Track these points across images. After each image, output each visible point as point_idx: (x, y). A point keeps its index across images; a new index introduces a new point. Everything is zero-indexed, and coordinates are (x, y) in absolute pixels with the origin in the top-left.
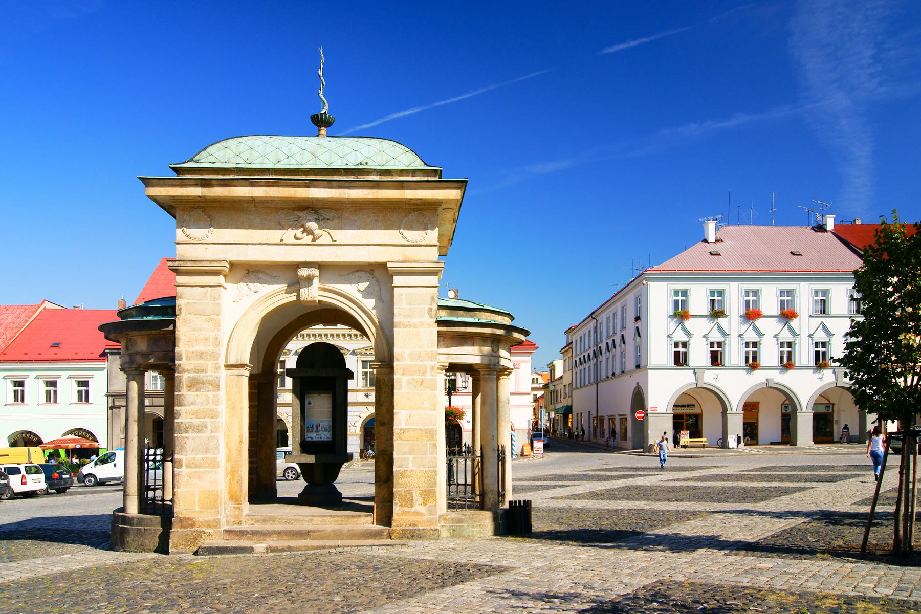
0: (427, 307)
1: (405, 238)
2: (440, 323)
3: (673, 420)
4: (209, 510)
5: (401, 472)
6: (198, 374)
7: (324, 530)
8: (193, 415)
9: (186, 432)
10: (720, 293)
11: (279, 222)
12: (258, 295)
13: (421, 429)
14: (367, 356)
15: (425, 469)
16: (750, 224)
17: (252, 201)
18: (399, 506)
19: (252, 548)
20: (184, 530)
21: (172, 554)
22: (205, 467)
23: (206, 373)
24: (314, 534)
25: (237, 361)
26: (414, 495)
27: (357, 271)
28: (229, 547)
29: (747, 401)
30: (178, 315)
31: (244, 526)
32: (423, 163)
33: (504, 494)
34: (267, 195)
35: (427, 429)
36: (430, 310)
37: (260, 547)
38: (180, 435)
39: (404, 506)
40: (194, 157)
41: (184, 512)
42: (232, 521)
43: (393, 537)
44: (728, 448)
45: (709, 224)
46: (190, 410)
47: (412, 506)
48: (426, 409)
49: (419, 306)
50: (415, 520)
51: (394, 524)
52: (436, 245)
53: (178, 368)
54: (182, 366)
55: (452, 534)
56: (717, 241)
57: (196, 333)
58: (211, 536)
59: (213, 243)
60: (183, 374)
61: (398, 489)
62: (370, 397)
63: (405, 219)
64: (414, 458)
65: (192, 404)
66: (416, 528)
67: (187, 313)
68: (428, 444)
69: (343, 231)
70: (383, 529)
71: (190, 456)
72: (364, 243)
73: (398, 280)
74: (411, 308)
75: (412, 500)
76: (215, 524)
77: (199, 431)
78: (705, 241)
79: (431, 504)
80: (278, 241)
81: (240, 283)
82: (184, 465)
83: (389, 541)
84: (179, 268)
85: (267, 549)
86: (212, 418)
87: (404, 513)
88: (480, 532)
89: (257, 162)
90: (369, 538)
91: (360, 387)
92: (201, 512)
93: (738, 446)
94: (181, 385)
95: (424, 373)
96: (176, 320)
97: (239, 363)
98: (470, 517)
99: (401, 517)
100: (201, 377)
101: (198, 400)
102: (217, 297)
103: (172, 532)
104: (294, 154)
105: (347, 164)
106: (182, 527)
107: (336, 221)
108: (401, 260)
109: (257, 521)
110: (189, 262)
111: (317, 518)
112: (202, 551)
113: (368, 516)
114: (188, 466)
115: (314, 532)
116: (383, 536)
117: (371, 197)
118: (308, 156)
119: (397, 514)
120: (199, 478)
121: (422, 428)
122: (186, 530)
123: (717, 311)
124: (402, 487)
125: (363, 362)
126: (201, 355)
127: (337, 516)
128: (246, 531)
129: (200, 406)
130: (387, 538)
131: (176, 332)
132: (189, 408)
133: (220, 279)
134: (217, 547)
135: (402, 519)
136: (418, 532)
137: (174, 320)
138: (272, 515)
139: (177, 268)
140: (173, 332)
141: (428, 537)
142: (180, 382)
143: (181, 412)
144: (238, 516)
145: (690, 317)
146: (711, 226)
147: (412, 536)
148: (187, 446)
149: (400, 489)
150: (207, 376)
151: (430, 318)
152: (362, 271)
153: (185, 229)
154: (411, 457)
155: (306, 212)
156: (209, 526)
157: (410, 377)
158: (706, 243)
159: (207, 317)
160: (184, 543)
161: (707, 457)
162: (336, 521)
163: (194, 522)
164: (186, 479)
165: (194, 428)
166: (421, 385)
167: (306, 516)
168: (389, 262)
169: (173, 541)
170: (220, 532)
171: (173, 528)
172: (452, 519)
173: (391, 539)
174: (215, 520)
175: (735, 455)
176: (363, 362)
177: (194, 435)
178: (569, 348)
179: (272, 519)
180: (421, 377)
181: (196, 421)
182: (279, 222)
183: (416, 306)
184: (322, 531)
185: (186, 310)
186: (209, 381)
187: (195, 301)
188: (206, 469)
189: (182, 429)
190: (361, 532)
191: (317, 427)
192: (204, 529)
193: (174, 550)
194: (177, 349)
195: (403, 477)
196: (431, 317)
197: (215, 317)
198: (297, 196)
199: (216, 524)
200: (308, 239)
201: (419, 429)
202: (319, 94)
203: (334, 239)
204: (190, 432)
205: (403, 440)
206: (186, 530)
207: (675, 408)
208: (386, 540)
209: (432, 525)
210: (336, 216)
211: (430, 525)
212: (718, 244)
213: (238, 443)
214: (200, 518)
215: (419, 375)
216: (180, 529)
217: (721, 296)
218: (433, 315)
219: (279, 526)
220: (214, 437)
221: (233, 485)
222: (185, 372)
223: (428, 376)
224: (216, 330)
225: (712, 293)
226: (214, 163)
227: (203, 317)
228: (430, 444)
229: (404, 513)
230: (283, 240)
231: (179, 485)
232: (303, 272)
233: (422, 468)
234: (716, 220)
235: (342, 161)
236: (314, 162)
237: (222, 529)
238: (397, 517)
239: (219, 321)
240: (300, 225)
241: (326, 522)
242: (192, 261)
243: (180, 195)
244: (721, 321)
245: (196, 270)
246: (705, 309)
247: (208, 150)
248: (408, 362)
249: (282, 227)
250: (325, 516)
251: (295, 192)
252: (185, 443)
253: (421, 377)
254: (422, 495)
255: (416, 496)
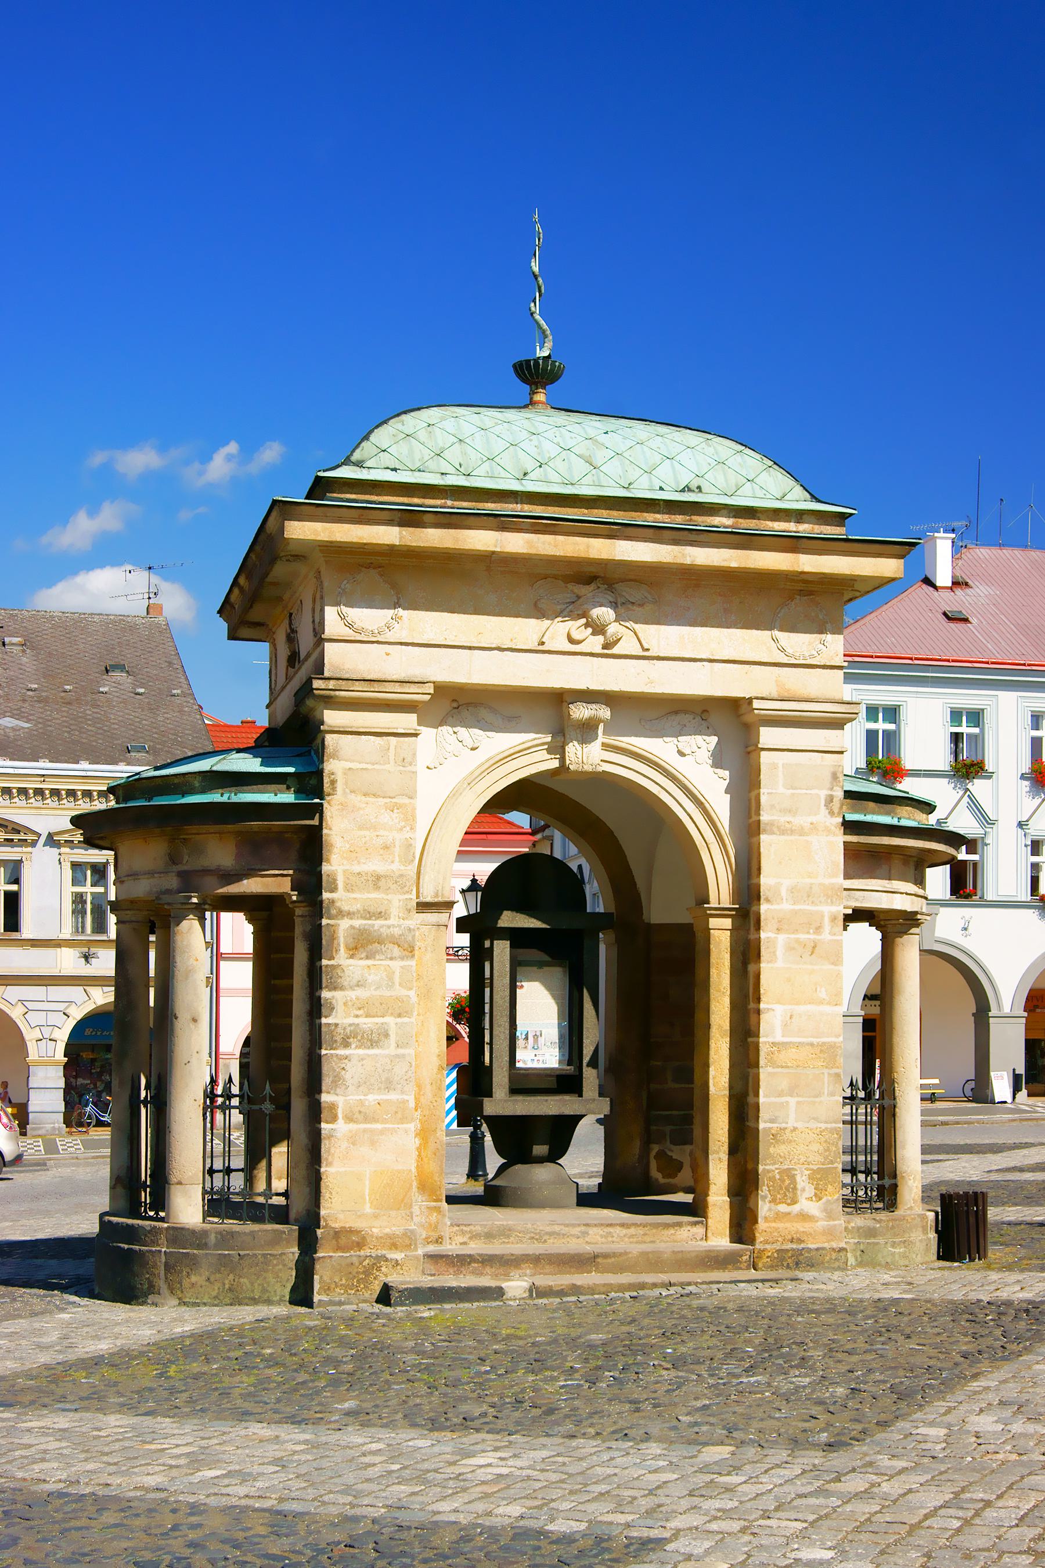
0: (823, 793)
1: (783, 650)
2: (849, 827)
3: (864, 1031)
4: (393, 1213)
5: (773, 1132)
6: (370, 922)
7: (626, 1253)
8: (360, 1009)
9: (346, 1045)
10: (976, 717)
11: (535, 605)
12: (480, 757)
13: (812, 1045)
14: (76, 851)
15: (820, 1125)
16: (1026, 547)
17: (489, 560)
18: (770, 1202)
19: (501, 1288)
20: (345, 1255)
21: (319, 1306)
22: (385, 1121)
23: (386, 919)
24: (605, 1261)
25: (437, 895)
26: (798, 1178)
27: (676, 712)
28: (453, 1288)
29: (1034, 988)
30: (329, 795)
31: (449, 1247)
32: (808, 494)
33: (896, 1186)
34: (533, 551)
35: (824, 1043)
36: (830, 799)
37: (516, 1286)
38: (332, 1052)
39: (778, 1201)
40: (351, 454)
41: (341, 1216)
42: (424, 1236)
43: (760, 1265)
44: (993, 1102)
45: (938, 541)
46: (354, 997)
47: (794, 1202)
48: (821, 1002)
49: (808, 792)
50: (802, 1229)
51: (760, 1238)
52: (841, 668)
53: (328, 909)
54: (338, 904)
55: (859, 1259)
56: (956, 583)
57: (367, 833)
58: (399, 1267)
59: (401, 644)
60: (339, 922)
61: (767, 1167)
62: (93, 961)
63: (783, 611)
64: (798, 1103)
65: (358, 986)
66: (802, 1246)
67: (348, 791)
68: (826, 1075)
69: (663, 628)
70: (742, 1250)
71: (354, 1097)
72: (704, 657)
73: (768, 736)
74: (793, 794)
75: (795, 1188)
76: (407, 1242)
77: (373, 1043)
78: (928, 582)
79: (830, 1198)
80: (533, 645)
81: (441, 725)
82: (340, 1115)
83: (752, 1274)
84: (337, 693)
85: (530, 1291)
86: (399, 1016)
87: (779, 1217)
88: (904, 1256)
89: (481, 471)
90: (713, 1269)
91: (67, 933)
92: (376, 1216)
93: (1014, 1098)
94: (335, 946)
95: (818, 929)
96: (326, 805)
97: (440, 899)
98: (888, 1227)
99: (774, 1225)
100: (376, 928)
101: (371, 978)
102: (408, 759)
103: (319, 1258)
104: (550, 459)
105: (661, 489)
106: (339, 1248)
107: (648, 607)
108: (775, 695)
109: (474, 1236)
110: (357, 683)
111: (595, 1229)
112: (400, 1297)
113: (695, 1224)
114: (349, 1119)
115: (606, 1256)
116: (741, 1262)
117: (734, 564)
118: (580, 467)
119: (766, 1218)
120: (373, 1143)
121: (815, 1041)
122: (348, 1255)
123: (968, 762)
124: (774, 1164)
125: (75, 866)
126: (377, 881)
127: (635, 1225)
128: (470, 1256)
129: (375, 989)
130: (748, 1268)
131: (325, 831)
132: (352, 994)
133: (407, 721)
134: (430, 1288)
135: (777, 1229)
136: (807, 1255)
137: (321, 805)
138: (505, 1223)
139: (332, 693)
140: (320, 828)
141: (826, 1265)
142: (333, 938)
143: (334, 1001)
144: (436, 1227)
145: (907, 775)
146: (943, 546)
147: (797, 1264)
148: (347, 1076)
149: (772, 1167)
150: (389, 927)
151: (829, 816)
152: (686, 712)
153: (344, 609)
154: (792, 1101)
155: (593, 586)
156: (394, 1246)
157: (793, 936)
158: (930, 588)
159: (388, 800)
160: (344, 1282)
161: (957, 1123)
162: (632, 1236)
163: (364, 1238)
164: (344, 1145)
165: (363, 1037)
166: (812, 953)
167: (574, 1225)
168: (757, 698)
169: (321, 1277)
170: (417, 1258)
171: (320, 1250)
172: (859, 1228)
173: (755, 1269)
174: (405, 1234)
175: (1021, 1120)
176: (75, 866)
177: (361, 1052)
178: (544, 838)
179: (505, 1232)
180: (812, 937)
181: (366, 1023)
182: (535, 605)
183: (804, 791)
184: (621, 1254)
185: (346, 783)
186: (393, 936)
187: (364, 766)
188: (387, 1126)
189: (338, 1038)
190: (697, 1256)
191: (536, 1037)
192: (384, 1252)
193: (325, 1298)
194: (326, 868)
195: (778, 1141)
196: (832, 813)
197: (406, 801)
198: (592, 557)
199: (405, 1241)
200: (595, 643)
201: (808, 1044)
202: (532, 314)
203: (646, 646)
204: (353, 1046)
205: (778, 1067)
206: (348, 1255)
207: (867, 1001)
208: (746, 1272)
209: (832, 1240)
210: (649, 596)
211: (828, 1241)
212: (959, 592)
213: (435, 1070)
214: (374, 1230)
215: (808, 933)
216: (334, 1252)
217: (977, 725)
218: (836, 810)
219: (519, 1245)
220: (404, 1056)
221: (426, 1160)
222: (343, 916)
223: (826, 936)
224: (408, 828)
225: (956, 715)
226: (395, 470)
227: (381, 799)
228: (829, 1074)
229: (779, 1217)
230: (543, 643)
231: (330, 1159)
232: (580, 712)
233: (813, 1124)
234: (953, 531)
235: (650, 479)
236: (595, 478)
237: (420, 1252)
238: (767, 1224)
239: (414, 809)
240: (580, 612)
241: (613, 1237)
242: (364, 680)
243: (355, 540)
244: (978, 787)
245: (370, 699)
246: (941, 758)
247: (373, 437)
248: (786, 906)
249: (539, 613)
250: (611, 1225)
251: (588, 547)
252: (343, 1068)
253: (812, 937)
254: (813, 1179)
255: (802, 1181)
